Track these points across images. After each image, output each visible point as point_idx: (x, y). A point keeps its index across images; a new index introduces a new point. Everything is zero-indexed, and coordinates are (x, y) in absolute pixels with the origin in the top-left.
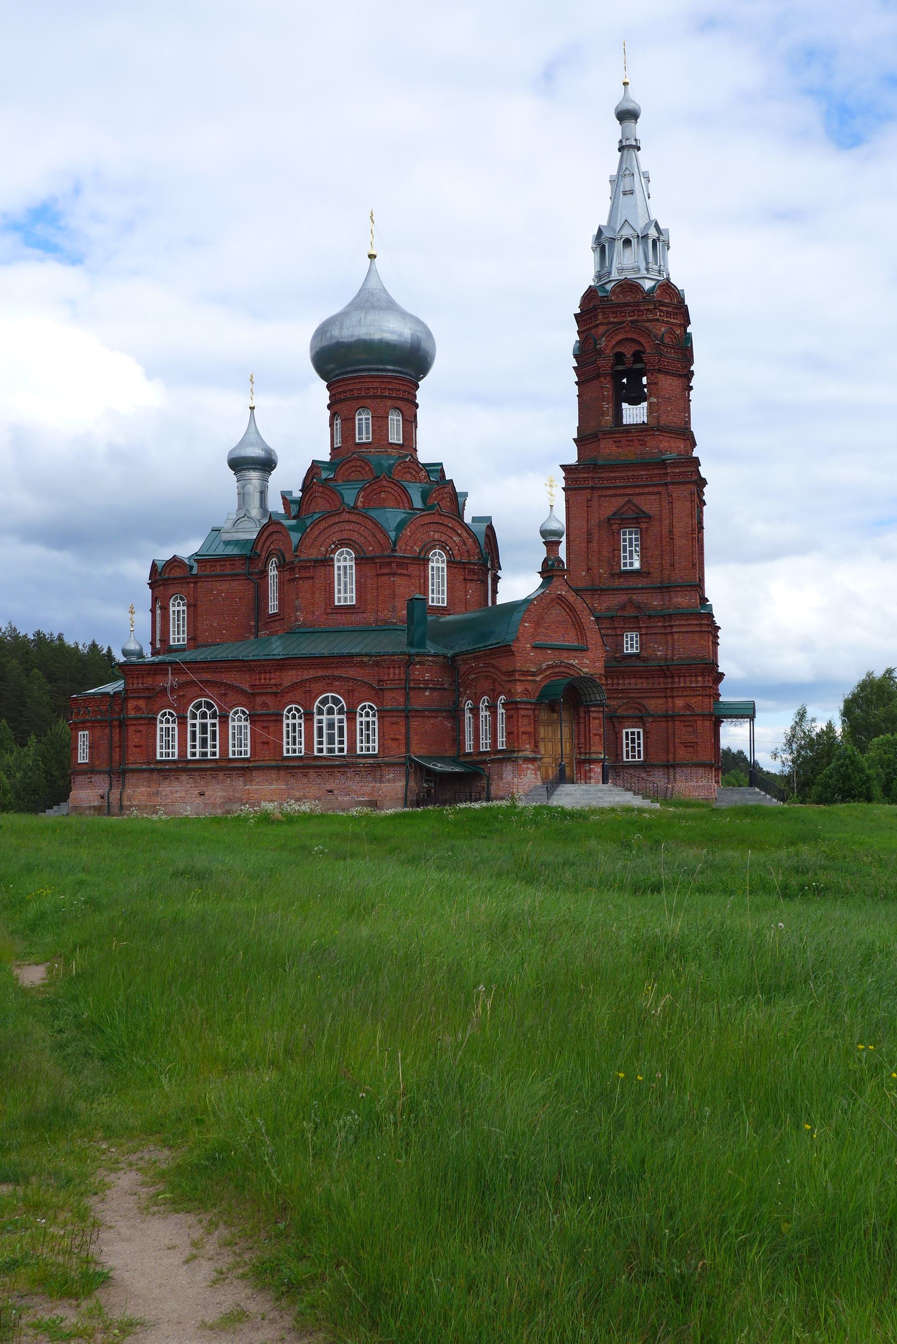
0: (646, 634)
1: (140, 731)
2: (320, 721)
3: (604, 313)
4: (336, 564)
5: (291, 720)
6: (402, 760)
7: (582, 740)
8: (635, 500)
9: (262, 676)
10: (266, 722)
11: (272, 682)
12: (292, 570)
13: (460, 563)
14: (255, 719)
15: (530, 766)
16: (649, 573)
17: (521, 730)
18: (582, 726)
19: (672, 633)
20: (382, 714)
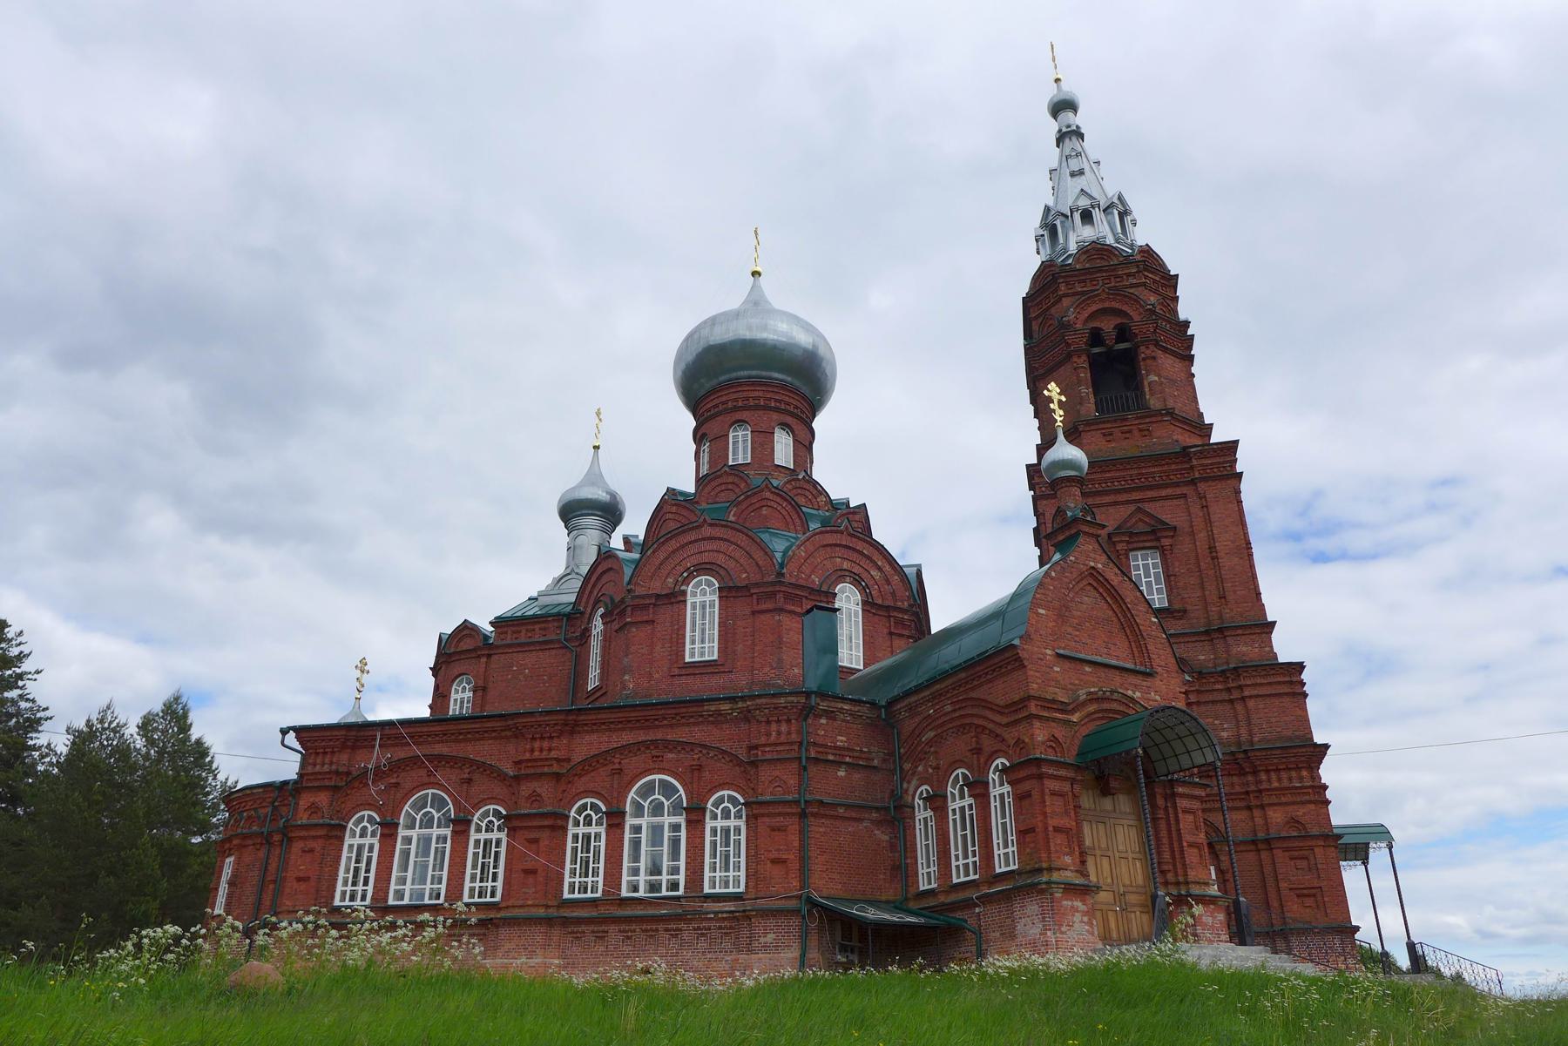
0: (1198, 703)
1: (311, 851)
2: (637, 829)
3: (1067, 283)
4: (690, 600)
5: (584, 826)
6: (793, 904)
7: (1167, 856)
8: (1147, 507)
9: (537, 745)
10: (537, 829)
11: (553, 754)
12: (622, 613)
13: (880, 607)
14: (516, 823)
15: (1078, 904)
16: (1185, 611)
17: (1052, 822)
18: (1163, 825)
19: (1243, 699)
20: (755, 811)
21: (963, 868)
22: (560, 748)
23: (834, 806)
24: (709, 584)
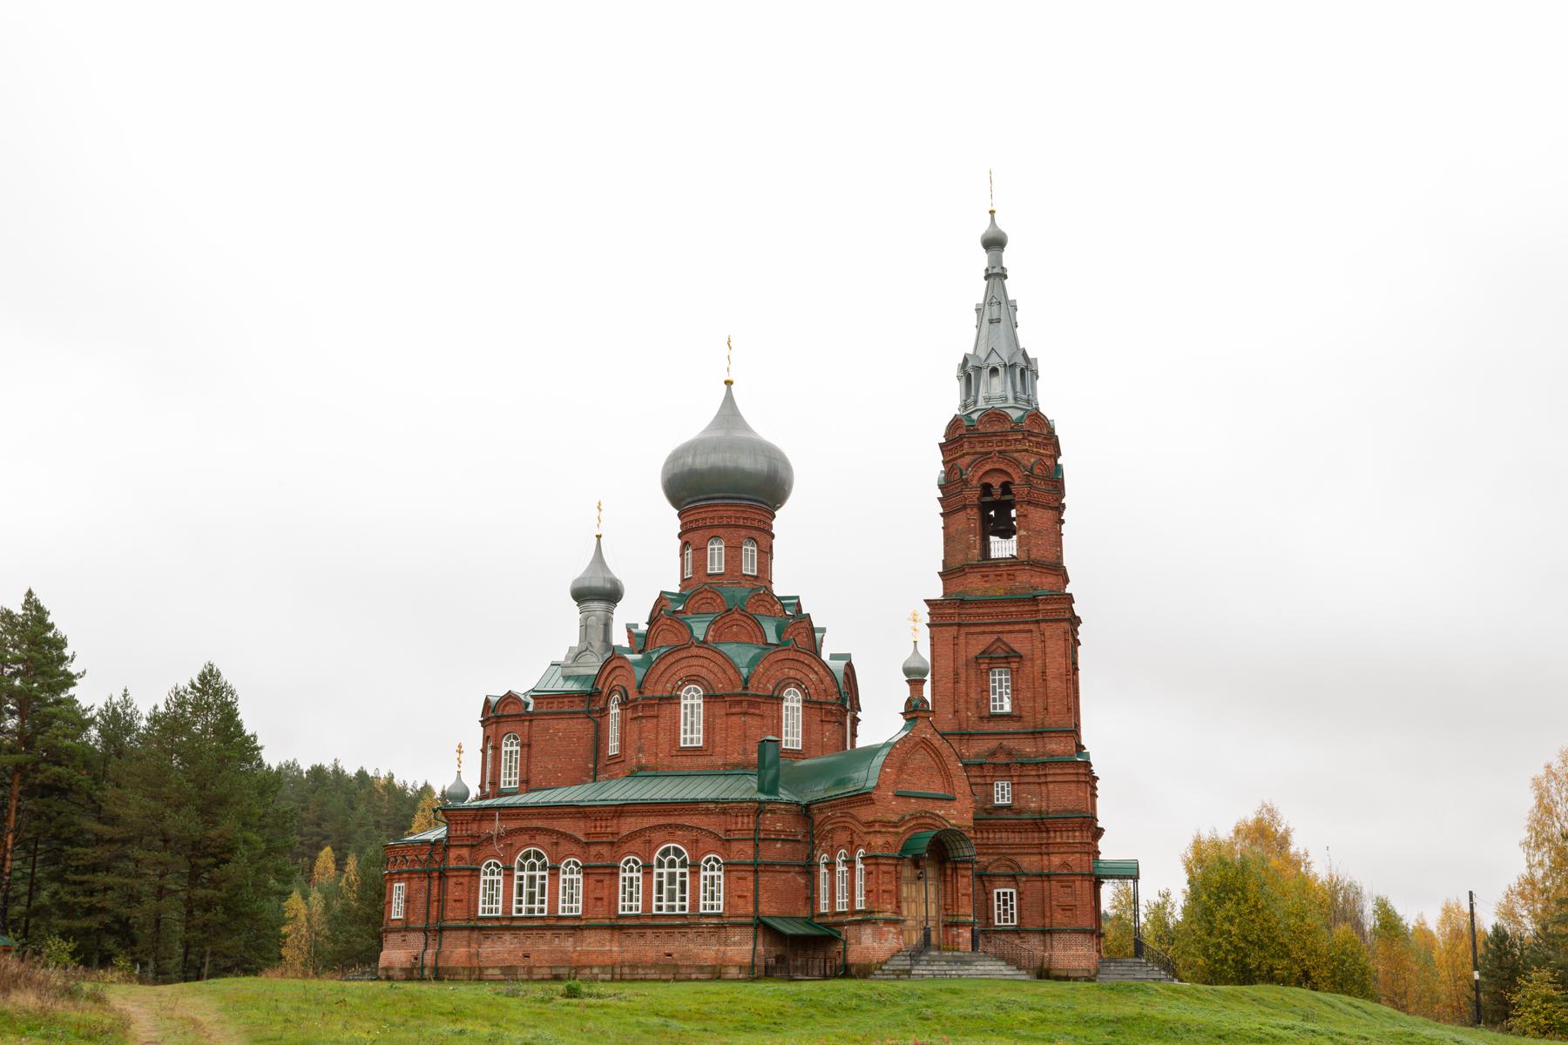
4: (683, 702)
5: (630, 874)
6: (749, 920)
10: (600, 873)
20: (729, 867)
21: (841, 904)
22: (612, 826)
23: (773, 865)
24: (696, 691)
